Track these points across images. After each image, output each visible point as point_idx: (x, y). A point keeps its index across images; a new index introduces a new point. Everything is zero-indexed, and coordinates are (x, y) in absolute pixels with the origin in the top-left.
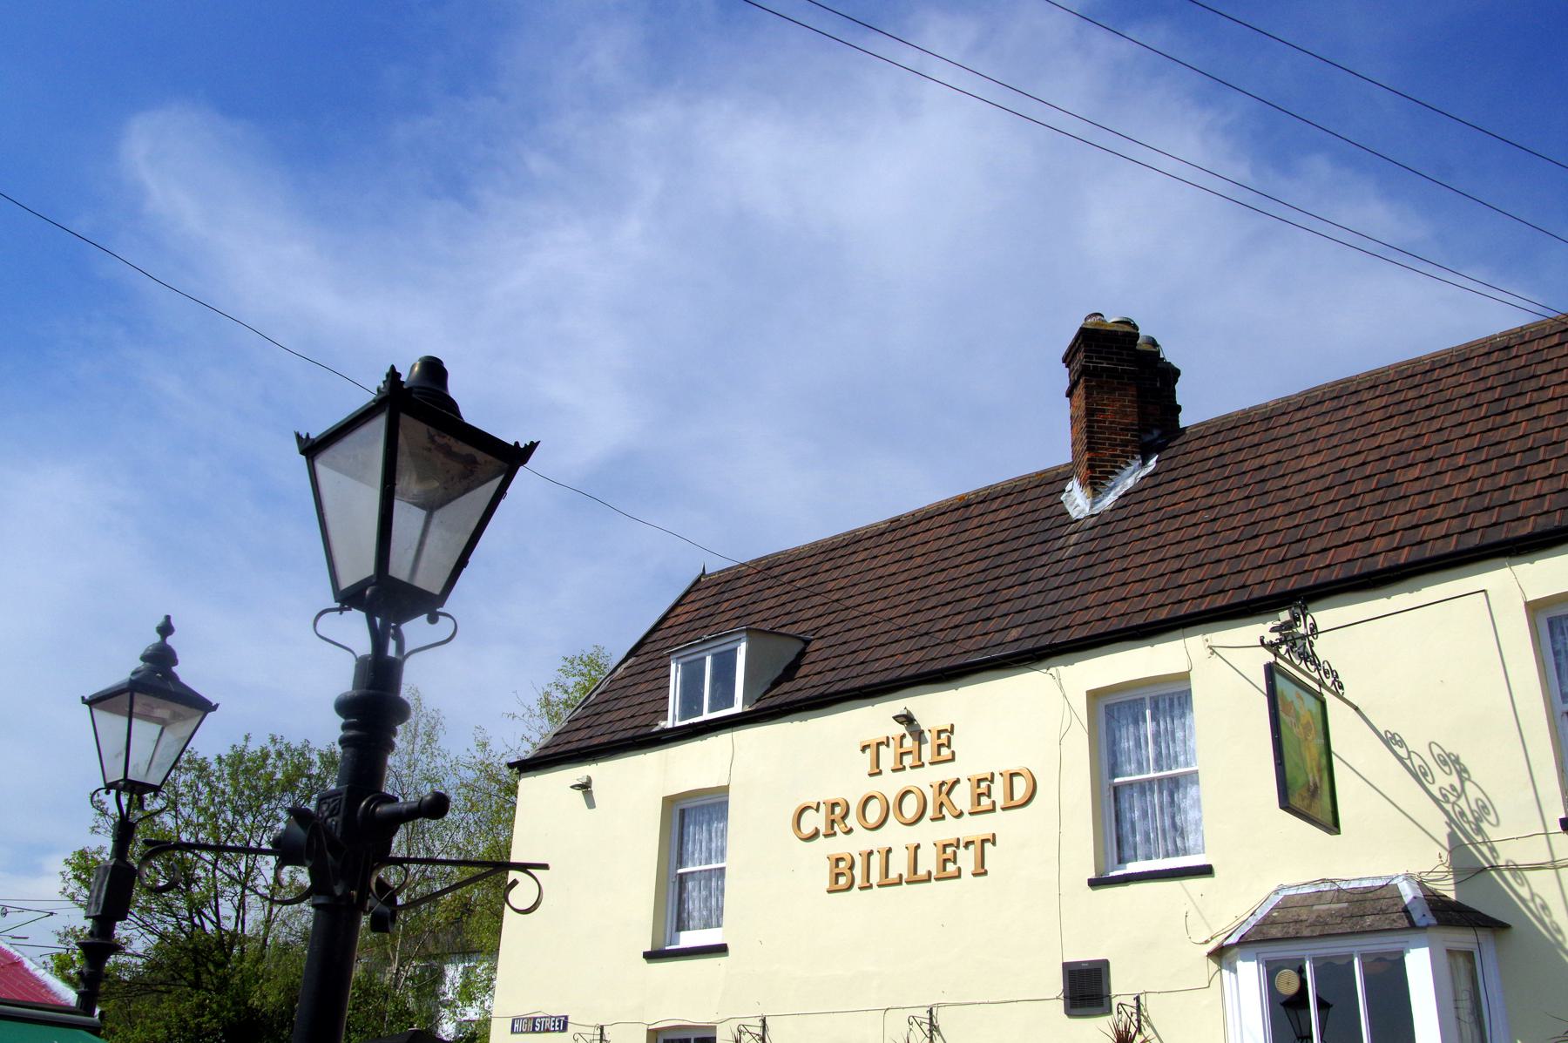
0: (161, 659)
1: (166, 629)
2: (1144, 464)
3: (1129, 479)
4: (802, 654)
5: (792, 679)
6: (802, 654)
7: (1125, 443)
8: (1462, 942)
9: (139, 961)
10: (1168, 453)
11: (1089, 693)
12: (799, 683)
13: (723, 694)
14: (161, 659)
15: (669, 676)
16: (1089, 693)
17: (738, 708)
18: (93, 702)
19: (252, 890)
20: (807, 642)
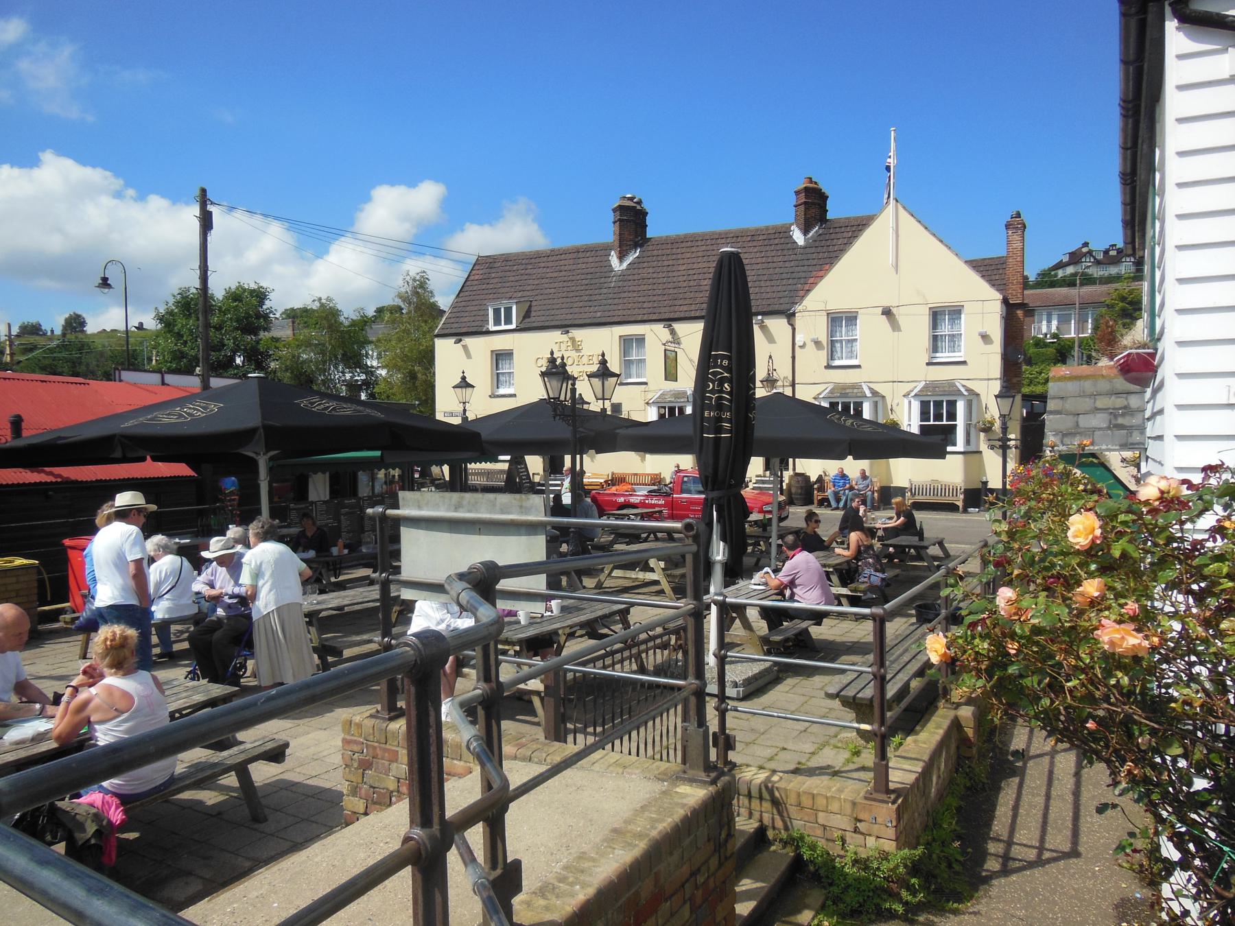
0: (464, 378)
1: (463, 373)
2: (635, 252)
3: (631, 258)
4: (530, 306)
5: (529, 317)
6: (530, 306)
7: (630, 245)
8: (759, 585)
9: (665, 465)
10: (643, 249)
11: (666, 379)
12: (532, 319)
13: (508, 320)
14: (464, 378)
15: (488, 315)
16: (666, 379)
17: (513, 326)
18: (453, 387)
19: (128, 344)
20: (531, 301)
